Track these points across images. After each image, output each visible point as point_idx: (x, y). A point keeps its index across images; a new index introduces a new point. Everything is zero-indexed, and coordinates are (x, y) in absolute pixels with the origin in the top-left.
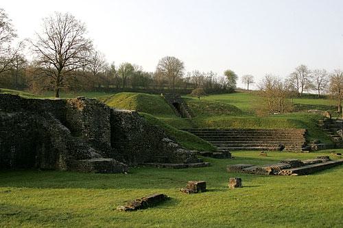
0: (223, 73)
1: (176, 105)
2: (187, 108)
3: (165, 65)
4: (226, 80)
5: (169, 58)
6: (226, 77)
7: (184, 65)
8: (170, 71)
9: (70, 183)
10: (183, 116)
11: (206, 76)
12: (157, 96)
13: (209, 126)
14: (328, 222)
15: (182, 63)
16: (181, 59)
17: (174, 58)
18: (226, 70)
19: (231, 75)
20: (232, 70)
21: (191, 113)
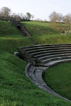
0: (26, 14)
1: (19, 27)
2: (26, 30)
3: (3, 10)
4: (27, 16)
5: (4, 8)
6: (27, 15)
7: (11, 10)
8: (5, 12)
9: (61, 21)
10: (26, 35)
11: (17, 14)
12: (7, 22)
13: (44, 43)
14: (66, 32)
15: (10, 10)
16: (9, 7)
17: (7, 8)
18: (27, 12)
19: (29, 14)
20: (30, 13)
21: (30, 33)
